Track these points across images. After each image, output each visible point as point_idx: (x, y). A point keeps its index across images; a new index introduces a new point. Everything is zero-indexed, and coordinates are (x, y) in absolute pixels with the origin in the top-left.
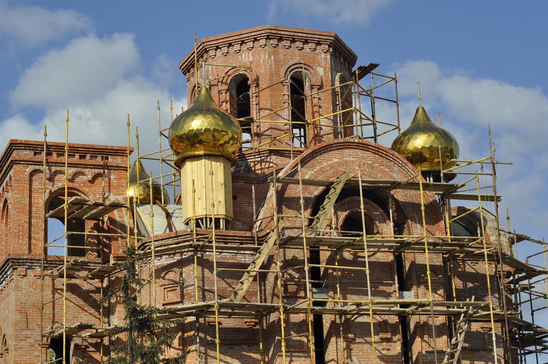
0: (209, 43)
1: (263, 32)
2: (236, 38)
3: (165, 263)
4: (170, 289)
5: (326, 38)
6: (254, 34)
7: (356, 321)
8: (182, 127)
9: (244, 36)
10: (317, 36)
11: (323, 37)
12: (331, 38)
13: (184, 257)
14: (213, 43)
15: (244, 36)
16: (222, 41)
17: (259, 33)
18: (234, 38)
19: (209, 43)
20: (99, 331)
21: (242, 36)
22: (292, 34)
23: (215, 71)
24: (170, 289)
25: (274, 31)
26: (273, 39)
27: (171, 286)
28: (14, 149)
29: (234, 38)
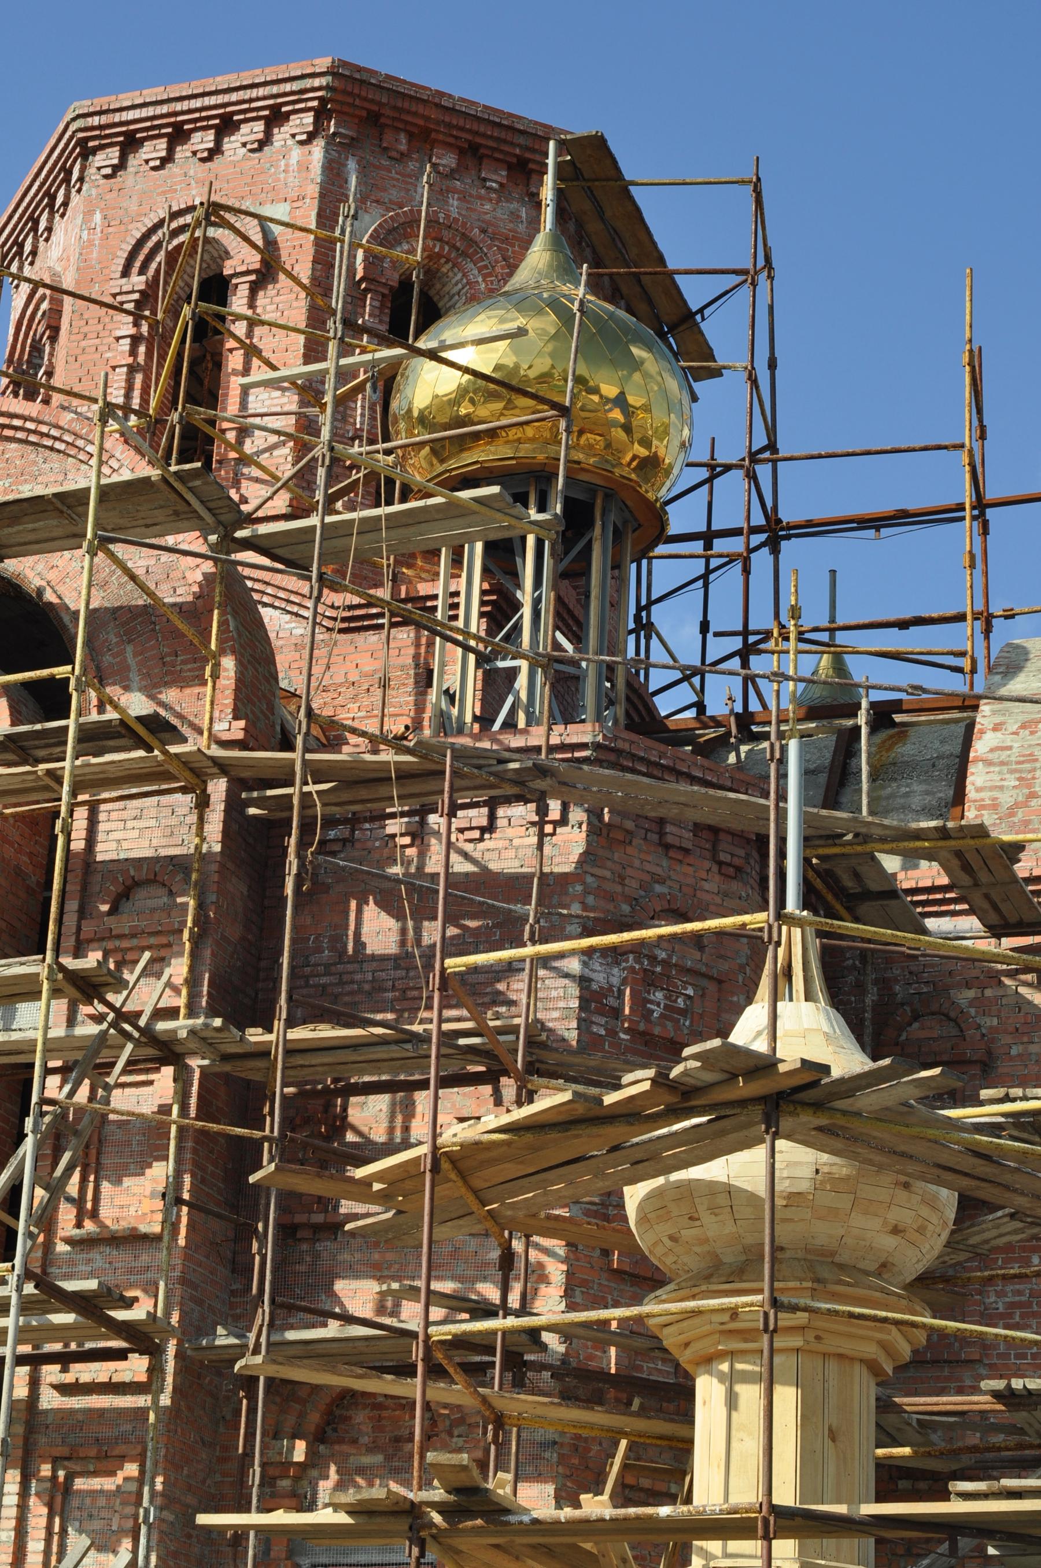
5: (296, 86)
7: (262, 610)
10: (261, 92)
11: (288, 87)
12: (317, 82)
22: (164, 109)
25: (95, 121)
26: (102, 147)
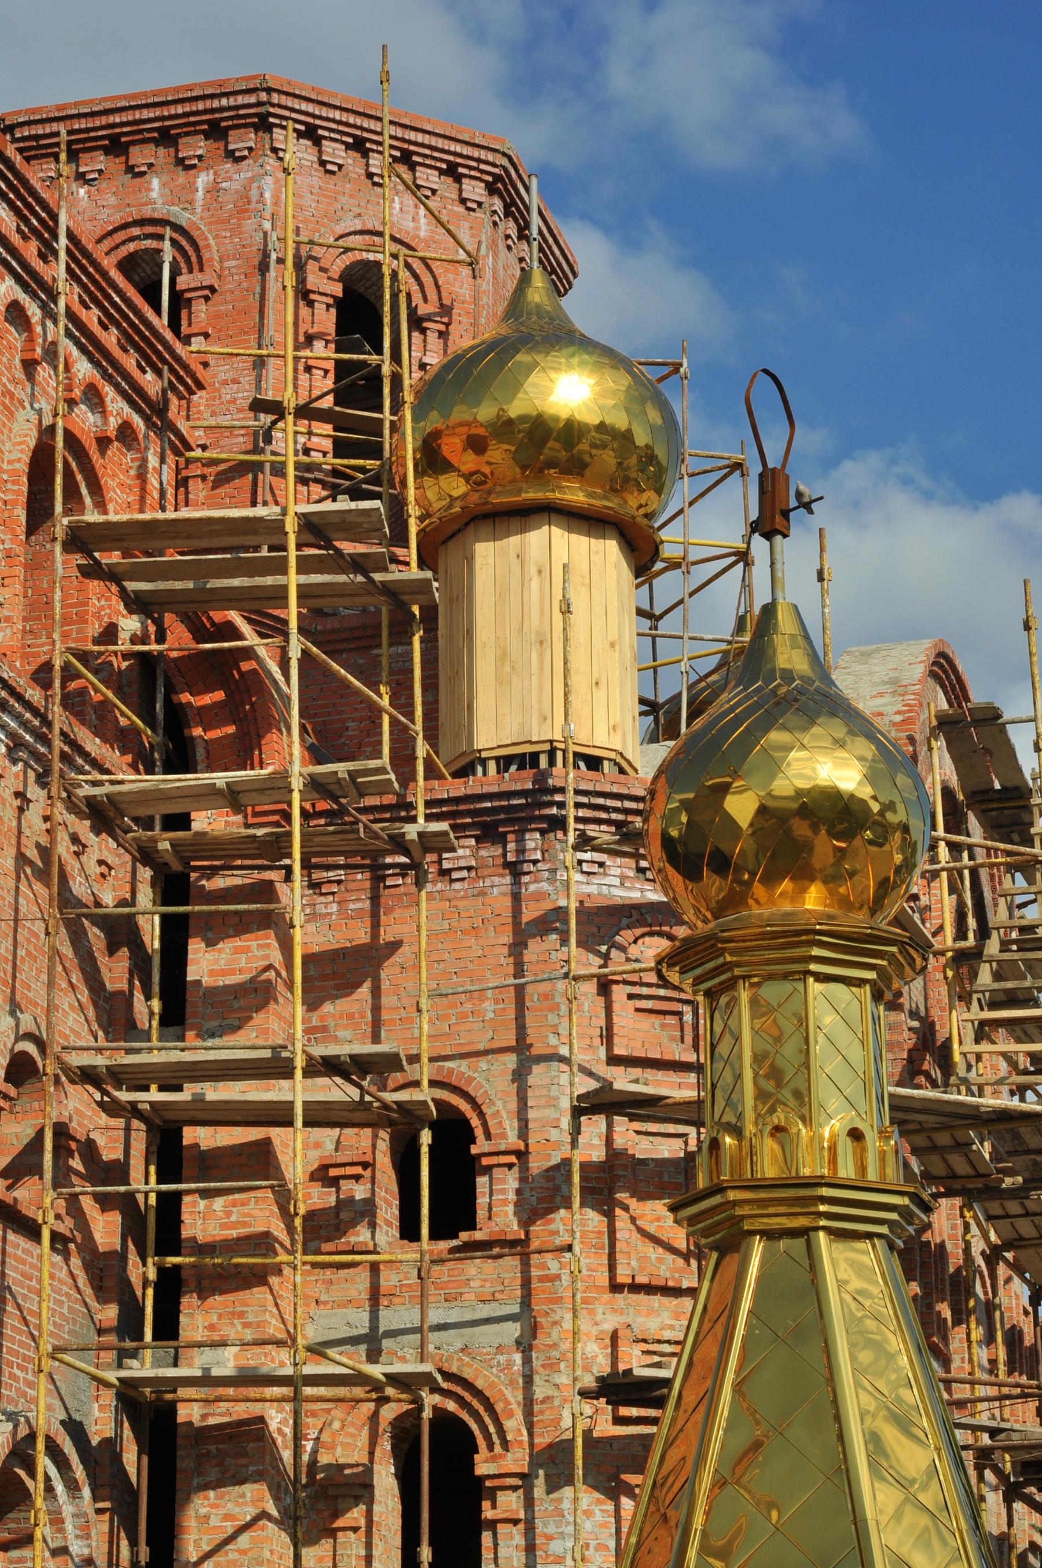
0: (290, 102)
1: (490, 157)
3: (616, 892)
4: (649, 1004)
8: (517, 386)
9: (420, 138)
15: (420, 138)
16: (337, 115)
17: (475, 153)
19: (290, 102)
21: (412, 136)
24: (649, 1004)
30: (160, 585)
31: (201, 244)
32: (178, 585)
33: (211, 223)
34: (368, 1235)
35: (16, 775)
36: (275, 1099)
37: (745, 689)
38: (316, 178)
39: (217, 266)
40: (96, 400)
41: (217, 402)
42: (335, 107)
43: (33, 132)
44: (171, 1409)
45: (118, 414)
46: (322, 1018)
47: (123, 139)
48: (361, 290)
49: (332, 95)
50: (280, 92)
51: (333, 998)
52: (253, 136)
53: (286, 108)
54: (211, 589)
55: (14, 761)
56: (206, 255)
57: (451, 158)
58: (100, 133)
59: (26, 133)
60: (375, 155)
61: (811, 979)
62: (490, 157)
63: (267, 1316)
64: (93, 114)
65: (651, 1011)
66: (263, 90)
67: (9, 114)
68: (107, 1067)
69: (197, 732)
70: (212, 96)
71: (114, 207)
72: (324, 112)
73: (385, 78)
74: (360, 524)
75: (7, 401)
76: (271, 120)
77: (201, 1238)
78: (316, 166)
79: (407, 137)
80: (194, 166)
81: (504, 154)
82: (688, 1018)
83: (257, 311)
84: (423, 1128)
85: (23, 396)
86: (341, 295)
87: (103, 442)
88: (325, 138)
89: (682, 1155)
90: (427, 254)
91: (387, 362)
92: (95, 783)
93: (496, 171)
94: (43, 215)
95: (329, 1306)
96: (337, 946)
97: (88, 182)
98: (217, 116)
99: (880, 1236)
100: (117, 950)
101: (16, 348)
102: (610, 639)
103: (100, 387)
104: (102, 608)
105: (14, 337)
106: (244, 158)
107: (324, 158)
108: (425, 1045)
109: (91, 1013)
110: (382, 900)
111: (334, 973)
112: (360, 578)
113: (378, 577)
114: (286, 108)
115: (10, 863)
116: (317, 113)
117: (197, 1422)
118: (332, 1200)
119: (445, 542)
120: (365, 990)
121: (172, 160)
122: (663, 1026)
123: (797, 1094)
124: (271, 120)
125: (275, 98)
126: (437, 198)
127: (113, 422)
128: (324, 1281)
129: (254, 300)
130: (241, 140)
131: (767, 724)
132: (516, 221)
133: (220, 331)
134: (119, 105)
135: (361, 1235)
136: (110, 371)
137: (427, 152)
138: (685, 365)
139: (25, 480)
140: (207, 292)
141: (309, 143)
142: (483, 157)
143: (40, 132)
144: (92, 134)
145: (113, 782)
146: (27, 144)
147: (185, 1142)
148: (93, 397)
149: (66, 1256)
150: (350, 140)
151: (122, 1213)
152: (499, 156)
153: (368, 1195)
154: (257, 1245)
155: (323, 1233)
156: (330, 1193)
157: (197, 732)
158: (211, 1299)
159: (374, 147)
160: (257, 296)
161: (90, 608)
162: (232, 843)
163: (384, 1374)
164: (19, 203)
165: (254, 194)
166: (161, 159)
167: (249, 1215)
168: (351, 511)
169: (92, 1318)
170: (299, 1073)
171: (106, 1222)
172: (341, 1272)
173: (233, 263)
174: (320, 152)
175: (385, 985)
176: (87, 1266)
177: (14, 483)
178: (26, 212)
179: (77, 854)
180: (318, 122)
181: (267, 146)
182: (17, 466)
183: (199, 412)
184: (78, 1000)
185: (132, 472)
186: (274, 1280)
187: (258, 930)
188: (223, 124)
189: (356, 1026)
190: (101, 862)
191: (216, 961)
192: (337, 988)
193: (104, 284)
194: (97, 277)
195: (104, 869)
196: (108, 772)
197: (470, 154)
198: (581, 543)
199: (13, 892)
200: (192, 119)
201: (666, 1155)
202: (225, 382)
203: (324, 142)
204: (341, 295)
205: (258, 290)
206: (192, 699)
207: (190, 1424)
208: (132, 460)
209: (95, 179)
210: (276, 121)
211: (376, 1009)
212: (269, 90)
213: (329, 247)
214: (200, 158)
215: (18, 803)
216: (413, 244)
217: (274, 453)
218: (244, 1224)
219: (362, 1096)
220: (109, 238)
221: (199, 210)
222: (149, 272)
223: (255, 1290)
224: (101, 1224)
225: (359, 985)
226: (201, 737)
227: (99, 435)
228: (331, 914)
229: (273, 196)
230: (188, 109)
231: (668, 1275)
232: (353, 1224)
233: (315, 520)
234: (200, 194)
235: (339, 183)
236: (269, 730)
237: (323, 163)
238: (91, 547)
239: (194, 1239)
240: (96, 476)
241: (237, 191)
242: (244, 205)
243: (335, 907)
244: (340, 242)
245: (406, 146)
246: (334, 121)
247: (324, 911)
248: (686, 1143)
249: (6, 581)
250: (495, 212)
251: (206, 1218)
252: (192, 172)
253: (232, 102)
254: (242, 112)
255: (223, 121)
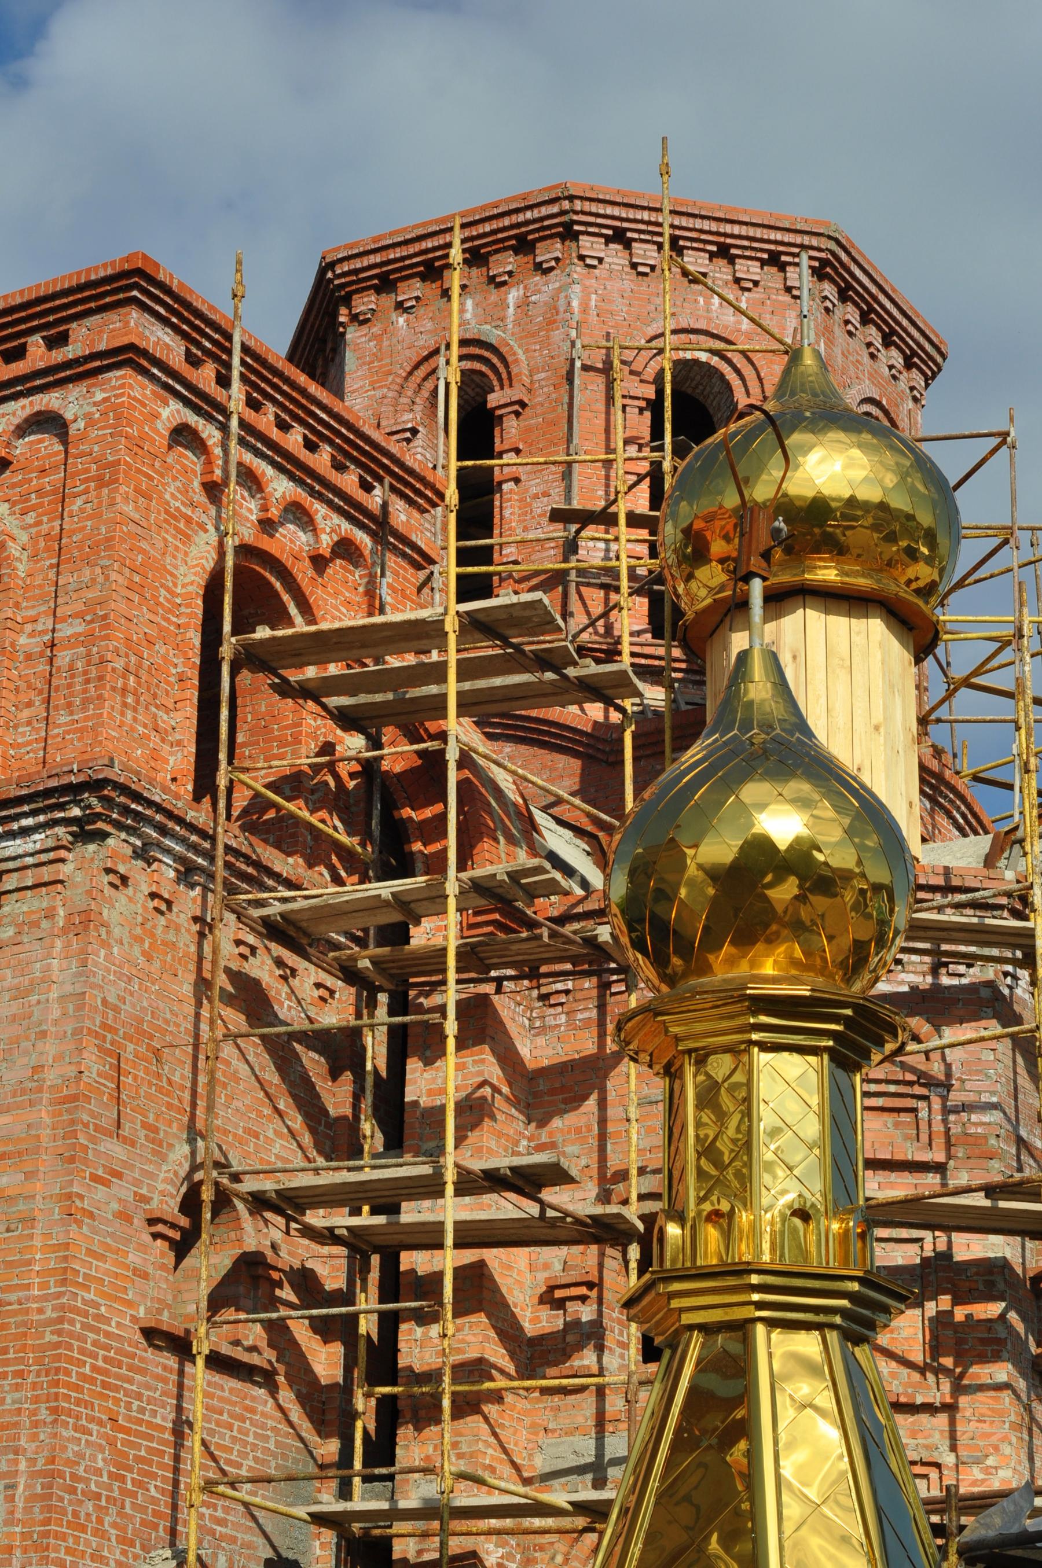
0: (594, 208)
1: (814, 242)
2: (706, 225)
4: (879, 1102)
6: (779, 236)
9: (736, 230)
13: (946, 981)
14: (609, 210)
15: (736, 230)
18: (699, 224)
19: (594, 208)
20: (550, 1213)
21: (728, 228)
23: (593, 318)
24: (879, 1102)
27: (892, 1088)
28: (135, 300)
29: (699, 224)
30: (363, 698)
31: (510, 359)
32: (379, 698)
33: (521, 338)
34: (594, 1358)
35: (194, 900)
36: (469, 1218)
37: (722, 736)
38: (628, 282)
39: (526, 380)
40: (305, 519)
41: (529, 517)
42: (643, 208)
43: (352, 267)
44: (386, 1543)
45: (333, 530)
46: (551, 1134)
47: (437, 264)
48: (689, 391)
49: (637, 196)
50: (581, 198)
51: (561, 1113)
52: (559, 246)
53: (590, 214)
54: (412, 699)
55: (192, 886)
56: (514, 370)
57: (772, 247)
58: (415, 260)
59: (346, 269)
60: (690, 252)
61: (756, 1049)
62: (814, 242)
63: (481, 1445)
64: (406, 242)
65: (882, 1109)
66: (566, 198)
67: (329, 252)
68: (276, 1191)
69: (417, 846)
70: (517, 211)
71: (430, 332)
72: (631, 214)
73: (665, 171)
74: (529, 619)
75: (182, 526)
76: (576, 228)
77: (418, 1368)
78: (628, 269)
79: (722, 230)
80: (505, 283)
81: (830, 237)
82: (923, 1114)
83: (565, 421)
84: (630, 1243)
85: (204, 518)
86: (653, 397)
87: (319, 562)
88: (635, 240)
89: (918, 1261)
90: (746, 347)
91: (669, 458)
92: (284, 900)
93: (823, 255)
94: (217, 336)
95: (556, 1435)
96: (565, 1059)
97: (407, 310)
98: (523, 229)
99: (833, 1326)
100: (340, 1075)
101: (194, 472)
102: (874, 722)
103: (307, 505)
104: (318, 728)
105: (190, 458)
106: (552, 269)
107: (635, 260)
108: (633, 1155)
109: (307, 1139)
110: (609, 1008)
111: (563, 1086)
112: (549, 675)
113: (571, 672)
114: (590, 214)
115: (187, 989)
116: (624, 215)
117: (412, 1558)
118: (560, 1324)
119: (711, 635)
120: (592, 1102)
121: (485, 280)
122: (897, 1125)
123: (738, 1174)
124: (576, 228)
125: (578, 205)
126: (760, 289)
127: (326, 541)
128: (552, 1408)
129: (563, 410)
130: (549, 251)
131: (744, 776)
132: (856, 304)
133: (531, 445)
134: (430, 230)
135: (587, 1358)
136: (317, 488)
137: (746, 243)
138: (1012, 434)
139: (200, 602)
140: (516, 407)
141: (619, 247)
142: (806, 243)
143: (359, 265)
144: (407, 262)
145: (306, 897)
146: (348, 279)
147: (402, 1268)
148: (298, 514)
149: (273, 1389)
150: (610, 232)
151: (344, 1344)
152: (824, 239)
153: (595, 1317)
154: (471, 1372)
155: (551, 1357)
156: (558, 1316)
157: (417, 846)
158: (427, 1430)
159: (688, 244)
160: (566, 406)
161: (304, 729)
162: (430, 957)
163: (570, 1503)
164: (185, 327)
165: (562, 304)
166: (475, 280)
167: (463, 1341)
168: (513, 605)
169: (311, 1453)
170: (450, 1189)
171: (328, 1353)
172: (569, 1398)
173: (543, 375)
174: (631, 254)
175: (611, 1096)
176: (302, 1399)
177: (188, 606)
178: (194, 335)
179: (284, 978)
180: (626, 225)
181: (574, 255)
182: (190, 588)
183: (510, 529)
184: (288, 1127)
185: (361, 589)
186: (491, 1409)
187: (474, 1045)
188: (530, 237)
189: (583, 1141)
190: (318, 985)
191: (434, 1080)
192: (565, 1101)
193: (304, 401)
194: (294, 394)
195: (322, 992)
196: (299, 888)
197: (792, 240)
198: (839, 623)
199: (191, 1019)
200: (500, 236)
201: (900, 1262)
202: (536, 496)
203: (634, 245)
204: (653, 397)
205: (566, 399)
206: (413, 814)
207: (405, 1560)
208: (361, 577)
209: (413, 307)
210: (636, 236)
211: (603, 1122)
212: (571, 198)
213: (640, 349)
214: (510, 273)
215: (197, 927)
216: (732, 338)
217: (578, 561)
218: (459, 1351)
219: (543, 1212)
220: (426, 364)
221: (510, 326)
222: (472, 394)
223: (469, 1419)
224: (324, 1356)
225: (586, 1097)
226: (421, 852)
227: (312, 554)
228: (559, 1026)
229: (580, 304)
230: (495, 226)
231: (901, 1390)
232: (579, 1347)
233: (481, 617)
234: (511, 310)
235: (652, 285)
236: (481, 840)
237: (634, 266)
238: (274, 665)
239: (410, 1368)
240: (303, 595)
241: (546, 303)
242: (554, 315)
243: (563, 1018)
244: (653, 344)
245: (722, 239)
246: (642, 222)
247: (553, 1023)
248: (922, 1248)
249: (178, 706)
250: (826, 298)
251: (419, 1347)
252: (503, 289)
253: (536, 214)
254: (546, 223)
255: (524, 236)
